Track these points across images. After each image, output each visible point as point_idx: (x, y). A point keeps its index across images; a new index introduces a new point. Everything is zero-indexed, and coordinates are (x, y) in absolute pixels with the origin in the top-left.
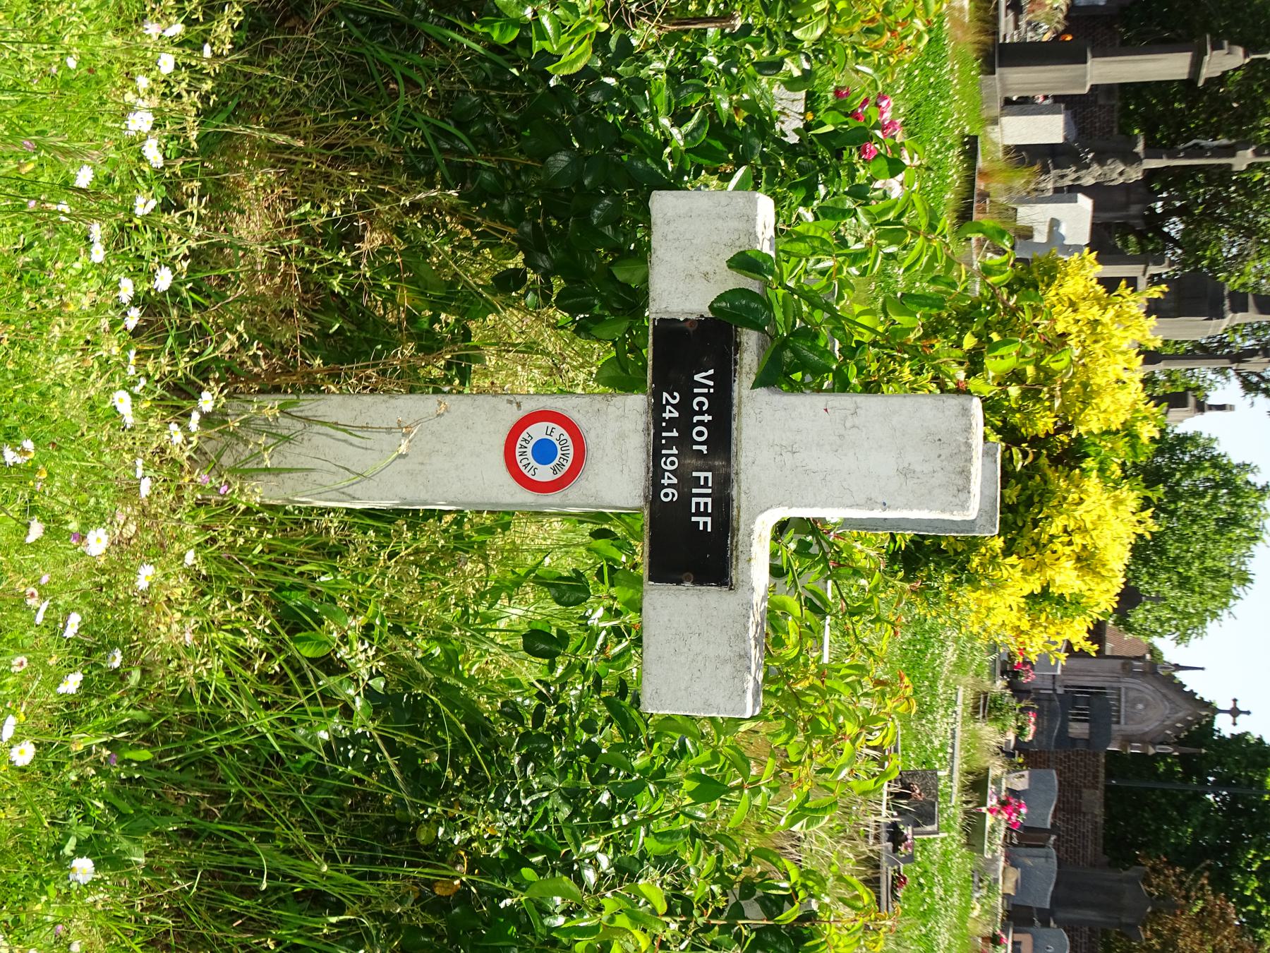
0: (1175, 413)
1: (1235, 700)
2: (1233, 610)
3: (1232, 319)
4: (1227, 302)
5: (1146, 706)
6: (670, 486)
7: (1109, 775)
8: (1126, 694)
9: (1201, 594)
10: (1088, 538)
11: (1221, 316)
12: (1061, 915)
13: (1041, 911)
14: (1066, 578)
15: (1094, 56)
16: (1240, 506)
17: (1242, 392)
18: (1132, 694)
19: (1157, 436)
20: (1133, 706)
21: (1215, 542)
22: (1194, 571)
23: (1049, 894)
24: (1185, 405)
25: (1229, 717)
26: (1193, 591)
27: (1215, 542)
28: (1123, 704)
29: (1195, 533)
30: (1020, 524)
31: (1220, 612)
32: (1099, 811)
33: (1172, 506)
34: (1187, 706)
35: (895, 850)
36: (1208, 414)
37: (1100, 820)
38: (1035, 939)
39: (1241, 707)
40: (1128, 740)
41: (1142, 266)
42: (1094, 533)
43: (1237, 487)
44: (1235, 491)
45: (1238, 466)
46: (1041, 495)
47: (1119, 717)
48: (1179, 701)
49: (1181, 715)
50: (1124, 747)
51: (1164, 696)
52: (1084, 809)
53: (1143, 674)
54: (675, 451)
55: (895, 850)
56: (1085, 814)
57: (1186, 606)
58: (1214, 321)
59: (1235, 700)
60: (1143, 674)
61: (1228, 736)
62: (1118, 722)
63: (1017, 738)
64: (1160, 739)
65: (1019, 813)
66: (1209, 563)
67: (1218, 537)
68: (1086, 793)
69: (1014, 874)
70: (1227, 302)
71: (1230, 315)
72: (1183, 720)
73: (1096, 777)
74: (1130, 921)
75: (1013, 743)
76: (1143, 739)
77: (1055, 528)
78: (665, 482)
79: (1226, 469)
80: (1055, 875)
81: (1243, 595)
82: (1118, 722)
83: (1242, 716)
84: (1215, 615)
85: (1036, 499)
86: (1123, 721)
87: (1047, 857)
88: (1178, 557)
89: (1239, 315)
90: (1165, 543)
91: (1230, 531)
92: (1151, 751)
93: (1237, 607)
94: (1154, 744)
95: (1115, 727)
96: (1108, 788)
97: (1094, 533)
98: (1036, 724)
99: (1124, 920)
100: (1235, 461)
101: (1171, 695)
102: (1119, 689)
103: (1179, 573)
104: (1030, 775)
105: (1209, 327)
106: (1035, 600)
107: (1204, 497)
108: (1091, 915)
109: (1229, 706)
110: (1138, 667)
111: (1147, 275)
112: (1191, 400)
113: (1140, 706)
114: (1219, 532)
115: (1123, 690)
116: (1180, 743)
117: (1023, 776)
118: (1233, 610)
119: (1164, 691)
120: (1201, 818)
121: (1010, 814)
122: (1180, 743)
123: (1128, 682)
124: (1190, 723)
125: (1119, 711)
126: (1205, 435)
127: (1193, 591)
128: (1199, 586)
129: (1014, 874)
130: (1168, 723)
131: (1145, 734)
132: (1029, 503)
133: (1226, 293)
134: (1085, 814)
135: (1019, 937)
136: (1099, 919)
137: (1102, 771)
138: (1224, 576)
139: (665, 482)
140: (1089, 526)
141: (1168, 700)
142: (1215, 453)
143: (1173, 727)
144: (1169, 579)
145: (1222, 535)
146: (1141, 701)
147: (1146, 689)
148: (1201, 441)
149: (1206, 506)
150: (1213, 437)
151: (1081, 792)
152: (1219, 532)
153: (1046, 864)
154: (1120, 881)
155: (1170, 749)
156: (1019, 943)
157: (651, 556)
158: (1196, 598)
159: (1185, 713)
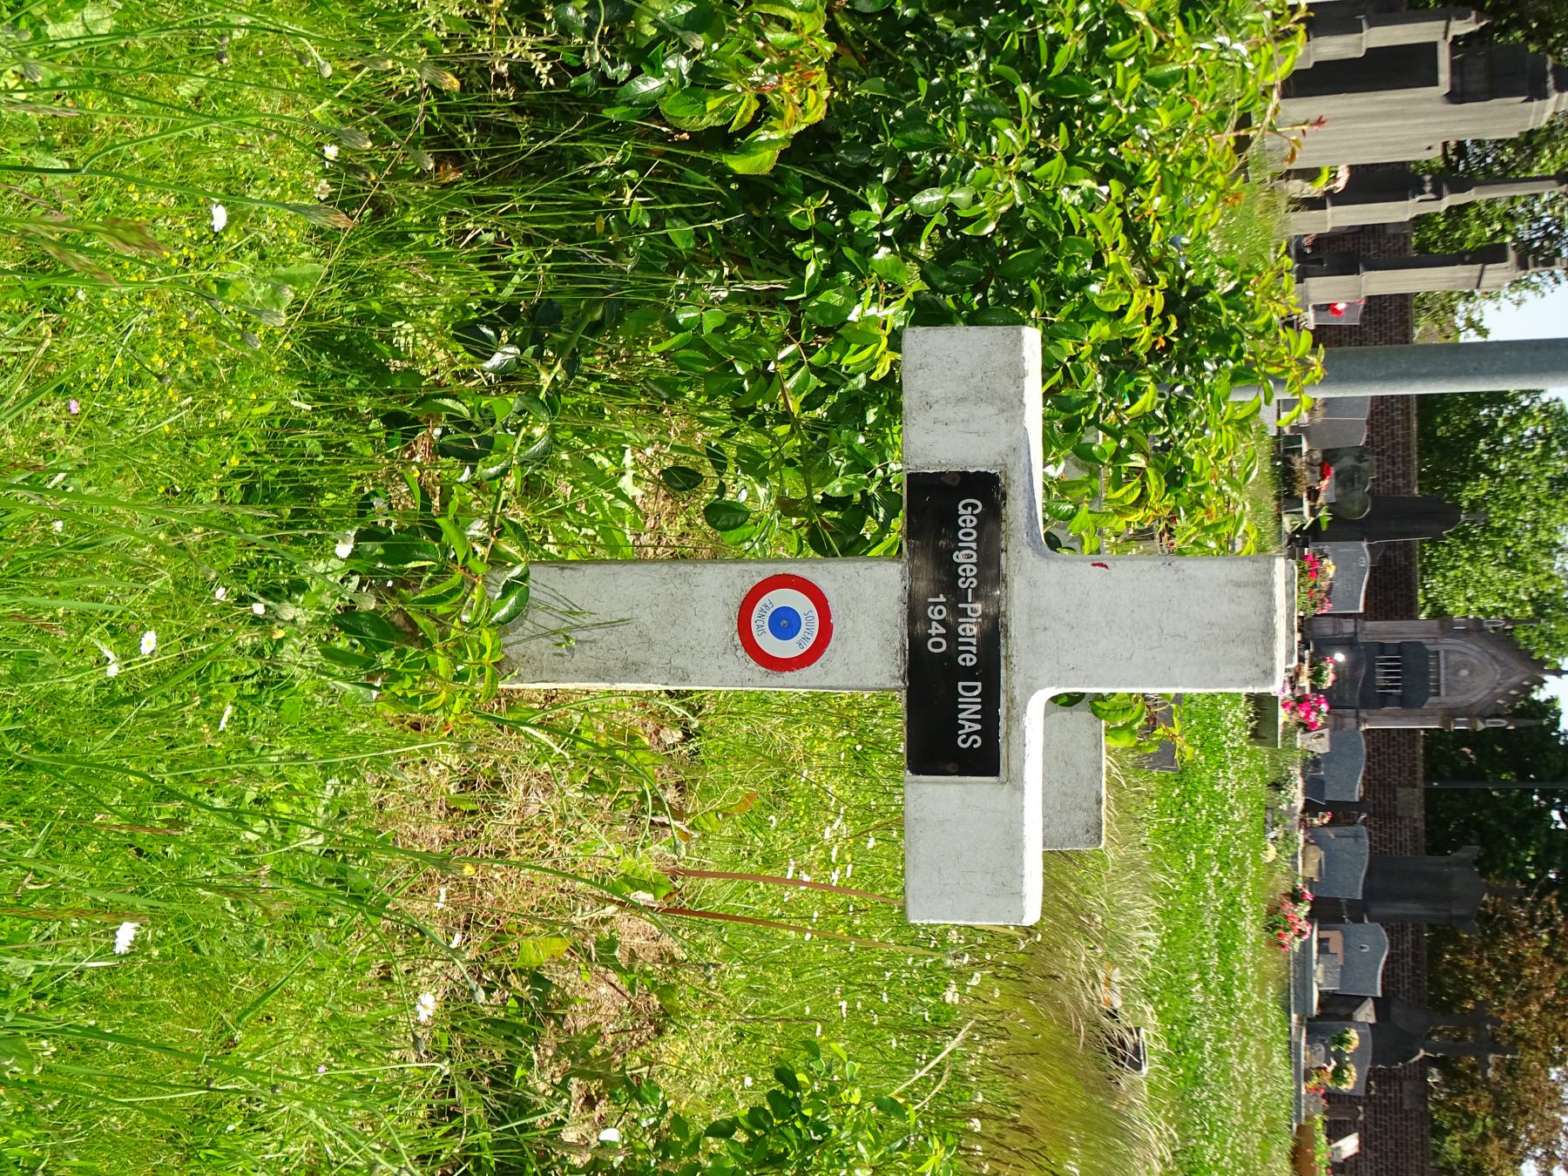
3: (1558, 101)
4: (1550, 79)
6: (938, 635)
7: (1428, 778)
9: (1536, 573)
11: (1544, 96)
12: (1377, 910)
13: (1352, 903)
15: (1371, 25)
17: (1561, 706)
18: (1454, 658)
19: (1471, 851)
20: (1456, 673)
21: (1549, 507)
22: (1525, 544)
23: (1361, 881)
26: (1524, 570)
27: (1549, 507)
28: (1443, 672)
32: (1418, 814)
37: (1421, 825)
38: (1345, 937)
40: (1451, 714)
41: (1443, 23)
47: (1438, 687)
48: (1513, 663)
49: (1515, 680)
50: (1446, 723)
51: (1494, 657)
52: (1399, 813)
53: (1466, 632)
54: (942, 599)
56: (1401, 818)
58: (1536, 103)
60: (1466, 632)
62: (1438, 694)
64: (1489, 711)
65: (1319, 712)
67: (1553, 502)
68: (1402, 793)
69: (1316, 855)
70: (1550, 79)
71: (1555, 96)
73: (1413, 772)
76: (1469, 712)
78: (933, 632)
80: (1366, 859)
82: (1438, 694)
86: (1443, 692)
87: (1356, 837)
88: (1504, 527)
92: (1481, 726)
94: (1484, 718)
96: (1428, 792)
99: (1454, 912)
102: (1437, 653)
105: (1527, 114)
108: (1411, 908)
111: (1450, 39)
113: (1464, 672)
115: (1442, 654)
117: (1322, 735)
119: (1493, 651)
121: (1308, 713)
123: (1447, 644)
125: (1438, 680)
127: (1524, 570)
129: (1316, 855)
130: (1499, 690)
131: (1472, 705)
133: (1549, 67)
134: (1401, 818)
135: (1324, 934)
139: (933, 632)
141: (1498, 661)
143: (1505, 695)
144: (1494, 556)
146: (1465, 665)
147: (1471, 650)
153: (1357, 848)
154: (1448, 864)
155: (1503, 723)
156: (1327, 940)
158: (1530, 578)
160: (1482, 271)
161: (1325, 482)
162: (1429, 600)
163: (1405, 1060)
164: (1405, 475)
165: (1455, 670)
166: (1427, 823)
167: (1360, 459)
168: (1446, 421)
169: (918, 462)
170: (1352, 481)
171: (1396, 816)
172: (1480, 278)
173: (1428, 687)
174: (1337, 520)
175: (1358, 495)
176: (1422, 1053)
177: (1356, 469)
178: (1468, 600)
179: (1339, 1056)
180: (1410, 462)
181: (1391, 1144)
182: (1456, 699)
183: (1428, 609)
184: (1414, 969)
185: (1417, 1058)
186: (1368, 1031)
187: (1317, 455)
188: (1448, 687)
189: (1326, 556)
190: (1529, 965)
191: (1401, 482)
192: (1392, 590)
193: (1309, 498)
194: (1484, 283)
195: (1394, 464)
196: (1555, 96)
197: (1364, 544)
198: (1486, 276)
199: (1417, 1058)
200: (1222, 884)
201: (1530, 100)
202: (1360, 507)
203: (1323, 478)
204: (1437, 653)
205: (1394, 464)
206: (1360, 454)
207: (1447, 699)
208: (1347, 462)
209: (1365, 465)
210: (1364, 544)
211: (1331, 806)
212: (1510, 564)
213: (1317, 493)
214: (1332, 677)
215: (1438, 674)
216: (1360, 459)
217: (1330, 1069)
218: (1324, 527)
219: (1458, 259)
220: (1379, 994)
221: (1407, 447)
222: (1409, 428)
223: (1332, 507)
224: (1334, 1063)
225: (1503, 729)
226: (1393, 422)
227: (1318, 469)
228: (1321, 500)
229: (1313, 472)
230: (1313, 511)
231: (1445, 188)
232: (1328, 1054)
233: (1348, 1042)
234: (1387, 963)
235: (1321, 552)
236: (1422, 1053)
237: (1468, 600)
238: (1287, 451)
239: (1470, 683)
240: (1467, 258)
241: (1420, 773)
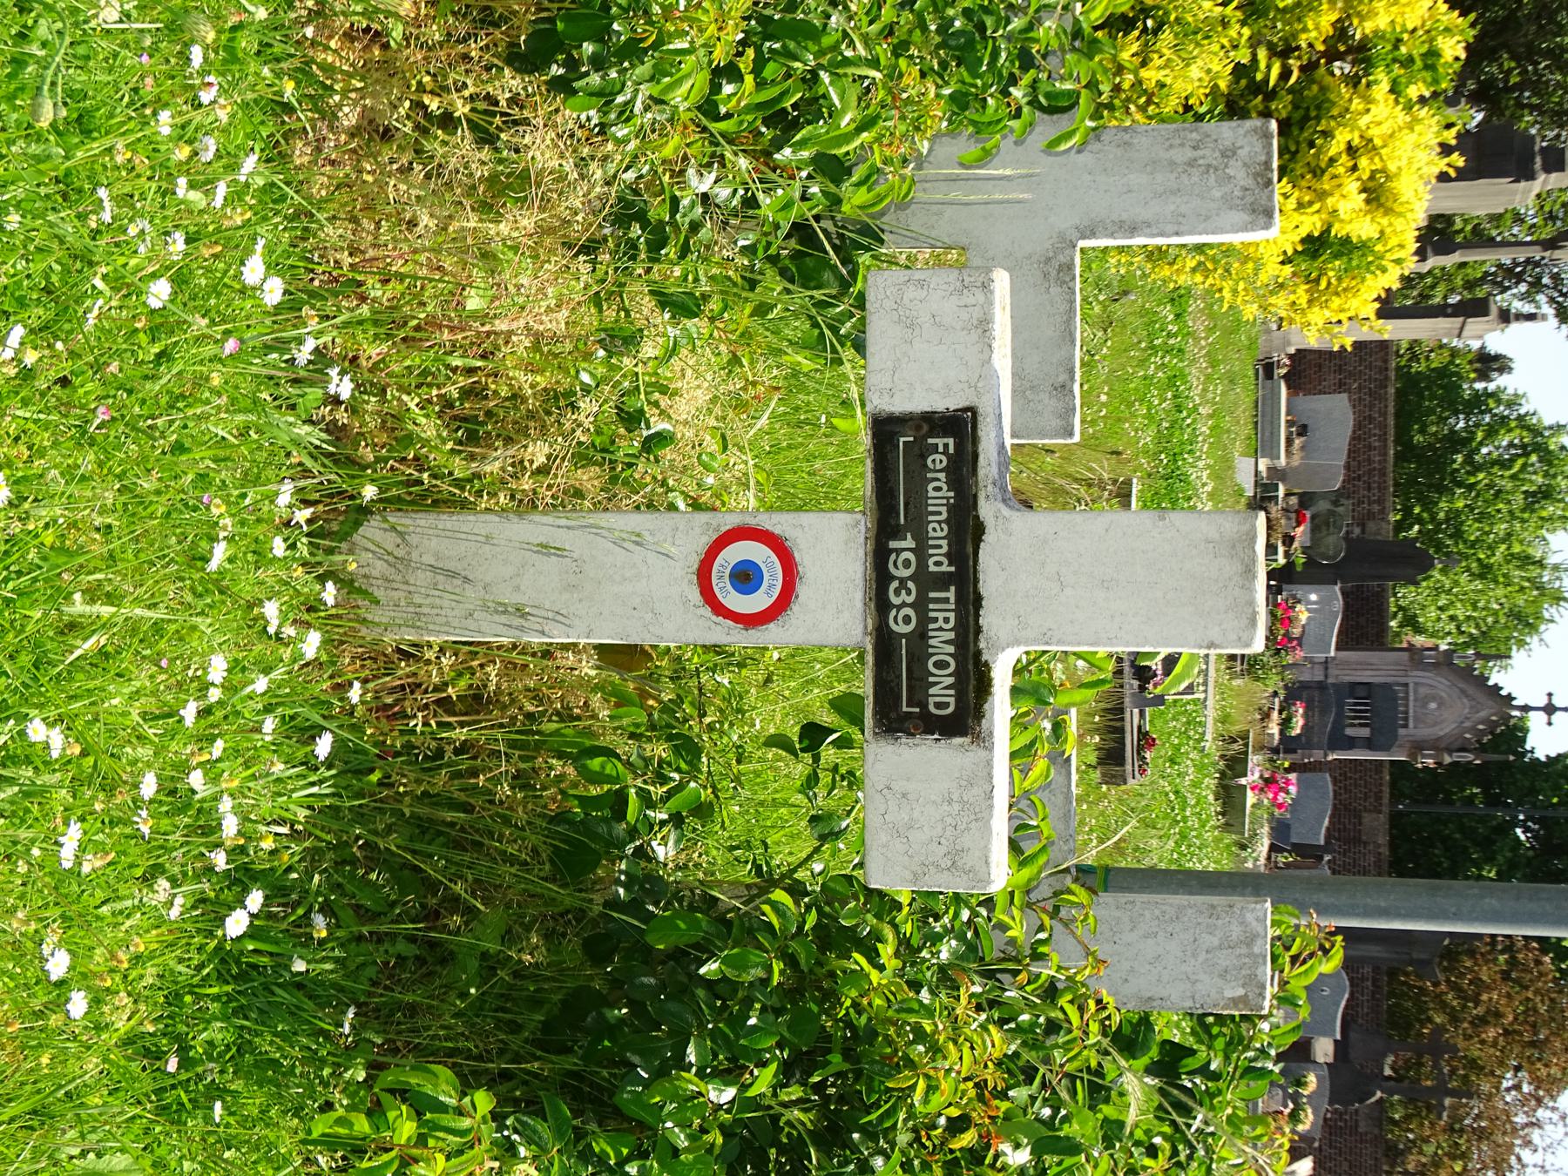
0: (1474, 325)
1: (1550, 695)
2: (1544, 636)
3: (1545, 181)
4: (1538, 160)
5: (1441, 705)
7: (1396, 796)
8: (1415, 692)
10: (1377, 159)
11: (1531, 176)
14: (1350, 213)
16: (1554, 476)
18: (1423, 691)
20: (1425, 705)
21: (1523, 521)
24: (1485, 313)
25: (1542, 716)
26: (1496, 582)
27: (1523, 521)
28: (1411, 704)
29: (1499, 511)
30: (1293, 148)
31: (1528, 640)
32: (1383, 840)
33: (1472, 480)
34: (1490, 703)
35: (1142, 688)
36: (1515, 327)
37: (1385, 851)
39: (1557, 702)
40: (1418, 747)
42: (1383, 151)
43: (1550, 452)
44: (1547, 457)
45: (1551, 428)
46: (1318, 107)
47: (1406, 719)
48: (1481, 697)
49: (1483, 714)
50: (1413, 756)
51: (1463, 691)
53: (1436, 665)
55: (1142, 688)
57: (1488, 602)
58: (1523, 184)
59: (1550, 695)
60: (1436, 665)
61: (1543, 759)
62: (1406, 726)
63: (1282, 732)
64: (1457, 745)
65: (1287, 793)
66: (1517, 549)
68: (1367, 818)
70: (1538, 160)
71: (1542, 177)
72: (1485, 721)
73: (1379, 798)
74: (1424, 956)
75: (1277, 737)
76: (1437, 746)
77: (1337, 146)
79: (1535, 431)
81: (1557, 617)
82: (1406, 726)
83: (1558, 714)
84: (1521, 643)
85: (1313, 114)
86: (1411, 724)
88: (1477, 540)
89: (1554, 175)
90: (1462, 523)
91: (1543, 508)
92: (1447, 760)
93: (1549, 632)
94: (1450, 751)
95: (1402, 731)
97: (1383, 151)
98: (1305, 715)
99: (1415, 956)
100: (1547, 423)
101: (1471, 690)
102: (1406, 685)
103: (1479, 560)
104: (1298, 779)
105: (1515, 193)
106: (1315, 246)
107: (1510, 468)
109: (1543, 702)
110: (1430, 657)
112: (1494, 310)
113: (1433, 705)
114: (1529, 508)
115: (1411, 686)
116: (1482, 749)
118: (1544, 636)
120: (1509, 855)
121: (1276, 794)
122: (1482, 749)
123: (1416, 676)
124: (1496, 724)
125: (1406, 713)
126: (1510, 391)
127: (1496, 582)
128: (1504, 575)
131: (1439, 739)
132: (1306, 119)
133: (1537, 148)
136: (1385, 955)
137: (1386, 790)
138: (1534, 563)
140: (1378, 142)
142: (1522, 411)
143: (1473, 729)
145: (1533, 511)
146: (1434, 699)
147: (1440, 683)
148: (1504, 397)
149: (1513, 477)
150: (1520, 392)
151: (1360, 817)
152: (1529, 508)
155: (1470, 757)
157: (875, 686)
158: (1500, 592)
159: (1488, 712)
160: (1464, 324)
161: (1301, 529)
162: (1401, 608)
163: (1361, 1101)
164: (1381, 501)
165: (1424, 702)
166: (1393, 845)
167: (1336, 503)
168: (1422, 431)
169: (859, 630)
170: (1328, 524)
171: (1360, 841)
172: (1462, 329)
173: (1397, 718)
174: (1311, 562)
175: (1331, 540)
176: (1379, 1094)
177: (1331, 513)
178: (1440, 609)
179: (1295, 1098)
180: (1386, 488)
181: (1345, 1166)
182: (1424, 732)
183: (1400, 615)
184: (1373, 993)
185: (1373, 1100)
186: (1326, 1072)
187: (1294, 500)
188: (1416, 719)
189: (1299, 602)
190: (1489, 988)
191: (1376, 508)
192: (1364, 625)
193: (1284, 543)
194: (1465, 333)
195: (1369, 489)
196: (1542, 177)
197: (1337, 588)
198: (1467, 328)
199: (1373, 1100)
200: (1178, 316)
201: (1517, 181)
202: (1334, 543)
203: (1299, 524)
204: (1406, 685)
205: (1369, 489)
206: (1337, 497)
207: (1414, 731)
208: (1323, 506)
209: (1340, 510)
210: (1337, 588)
211: (1299, 849)
212: (1482, 576)
213: (1292, 539)
214: (1301, 722)
215: (1407, 706)
216: (1336, 503)
217: (1287, 1111)
218: (1299, 569)
219: (1441, 311)
220: (1338, 1037)
221: (1383, 474)
222: (1385, 454)
223: (1305, 550)
224: (1291, 1106)
225: (1470, 763)
226: (1370, 448)
227: (1293, 516)
228: (1296, 544)
229: (1289, 519)
230: (1287, 554)
231: (1429, 250)
232: (1286, 1096)
233: (1305, 1084)
234: (1346, 1007)
235: (1294, 597)
236: (1379, 1094)
237: (1440, 609)
238: (1263, 498)
239: (1438, 720)
240: (1449, 310)
241: (1386, 801)
